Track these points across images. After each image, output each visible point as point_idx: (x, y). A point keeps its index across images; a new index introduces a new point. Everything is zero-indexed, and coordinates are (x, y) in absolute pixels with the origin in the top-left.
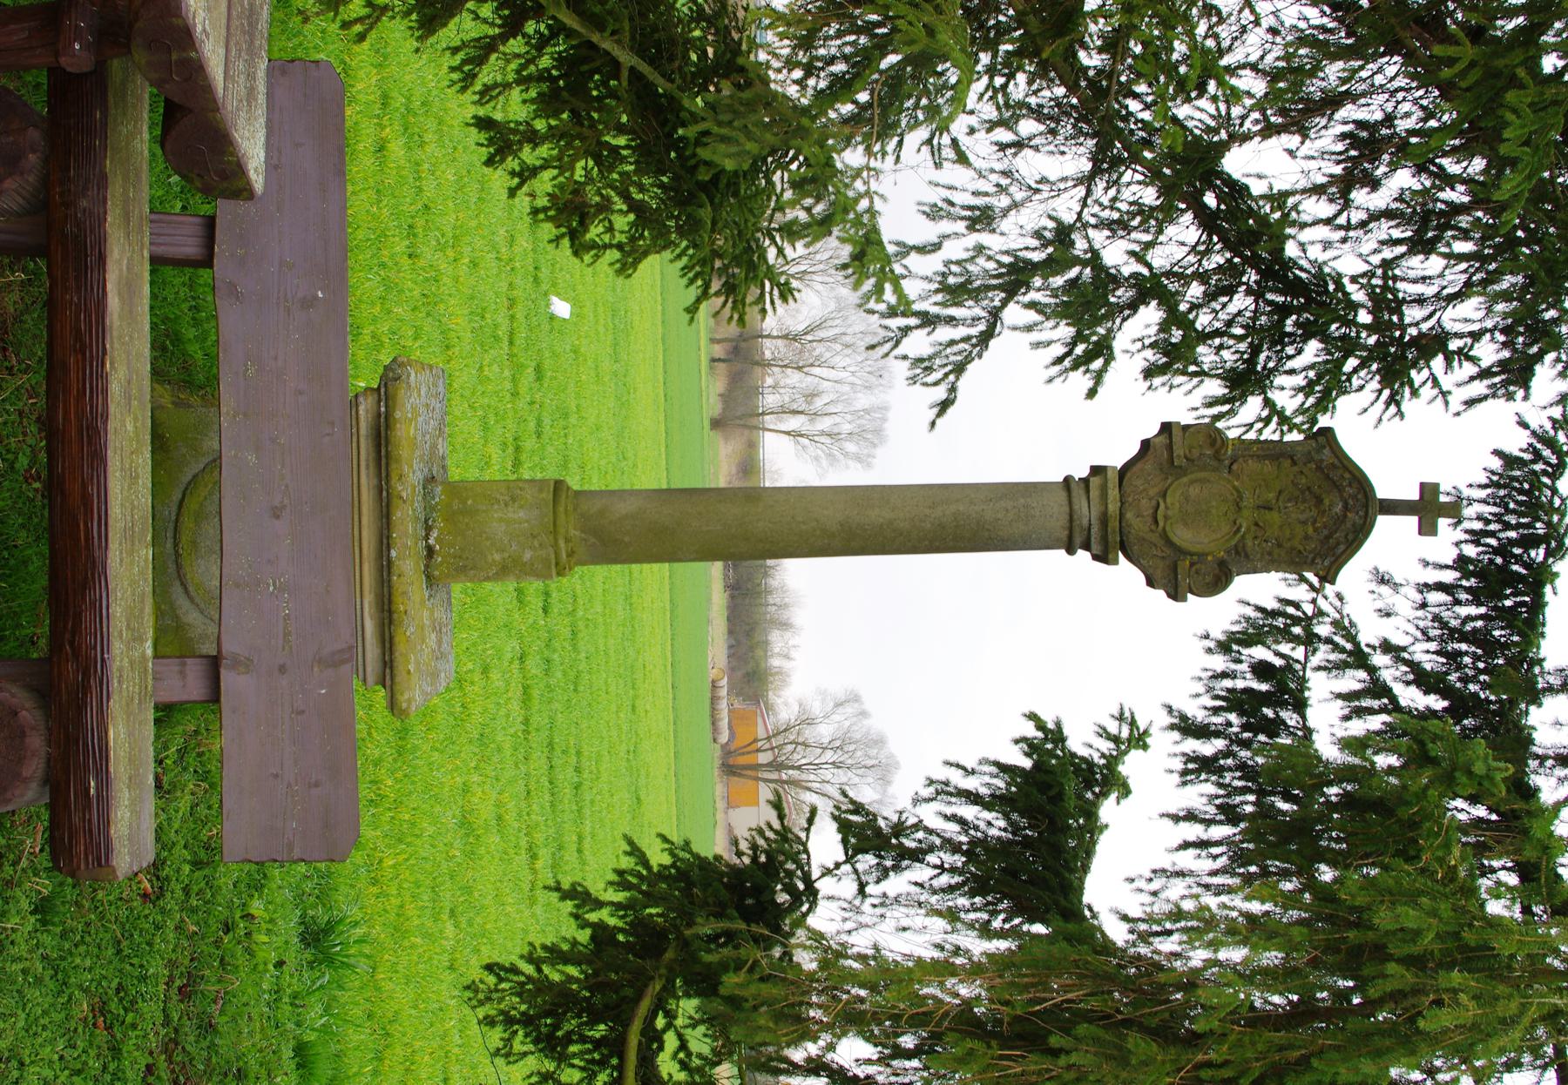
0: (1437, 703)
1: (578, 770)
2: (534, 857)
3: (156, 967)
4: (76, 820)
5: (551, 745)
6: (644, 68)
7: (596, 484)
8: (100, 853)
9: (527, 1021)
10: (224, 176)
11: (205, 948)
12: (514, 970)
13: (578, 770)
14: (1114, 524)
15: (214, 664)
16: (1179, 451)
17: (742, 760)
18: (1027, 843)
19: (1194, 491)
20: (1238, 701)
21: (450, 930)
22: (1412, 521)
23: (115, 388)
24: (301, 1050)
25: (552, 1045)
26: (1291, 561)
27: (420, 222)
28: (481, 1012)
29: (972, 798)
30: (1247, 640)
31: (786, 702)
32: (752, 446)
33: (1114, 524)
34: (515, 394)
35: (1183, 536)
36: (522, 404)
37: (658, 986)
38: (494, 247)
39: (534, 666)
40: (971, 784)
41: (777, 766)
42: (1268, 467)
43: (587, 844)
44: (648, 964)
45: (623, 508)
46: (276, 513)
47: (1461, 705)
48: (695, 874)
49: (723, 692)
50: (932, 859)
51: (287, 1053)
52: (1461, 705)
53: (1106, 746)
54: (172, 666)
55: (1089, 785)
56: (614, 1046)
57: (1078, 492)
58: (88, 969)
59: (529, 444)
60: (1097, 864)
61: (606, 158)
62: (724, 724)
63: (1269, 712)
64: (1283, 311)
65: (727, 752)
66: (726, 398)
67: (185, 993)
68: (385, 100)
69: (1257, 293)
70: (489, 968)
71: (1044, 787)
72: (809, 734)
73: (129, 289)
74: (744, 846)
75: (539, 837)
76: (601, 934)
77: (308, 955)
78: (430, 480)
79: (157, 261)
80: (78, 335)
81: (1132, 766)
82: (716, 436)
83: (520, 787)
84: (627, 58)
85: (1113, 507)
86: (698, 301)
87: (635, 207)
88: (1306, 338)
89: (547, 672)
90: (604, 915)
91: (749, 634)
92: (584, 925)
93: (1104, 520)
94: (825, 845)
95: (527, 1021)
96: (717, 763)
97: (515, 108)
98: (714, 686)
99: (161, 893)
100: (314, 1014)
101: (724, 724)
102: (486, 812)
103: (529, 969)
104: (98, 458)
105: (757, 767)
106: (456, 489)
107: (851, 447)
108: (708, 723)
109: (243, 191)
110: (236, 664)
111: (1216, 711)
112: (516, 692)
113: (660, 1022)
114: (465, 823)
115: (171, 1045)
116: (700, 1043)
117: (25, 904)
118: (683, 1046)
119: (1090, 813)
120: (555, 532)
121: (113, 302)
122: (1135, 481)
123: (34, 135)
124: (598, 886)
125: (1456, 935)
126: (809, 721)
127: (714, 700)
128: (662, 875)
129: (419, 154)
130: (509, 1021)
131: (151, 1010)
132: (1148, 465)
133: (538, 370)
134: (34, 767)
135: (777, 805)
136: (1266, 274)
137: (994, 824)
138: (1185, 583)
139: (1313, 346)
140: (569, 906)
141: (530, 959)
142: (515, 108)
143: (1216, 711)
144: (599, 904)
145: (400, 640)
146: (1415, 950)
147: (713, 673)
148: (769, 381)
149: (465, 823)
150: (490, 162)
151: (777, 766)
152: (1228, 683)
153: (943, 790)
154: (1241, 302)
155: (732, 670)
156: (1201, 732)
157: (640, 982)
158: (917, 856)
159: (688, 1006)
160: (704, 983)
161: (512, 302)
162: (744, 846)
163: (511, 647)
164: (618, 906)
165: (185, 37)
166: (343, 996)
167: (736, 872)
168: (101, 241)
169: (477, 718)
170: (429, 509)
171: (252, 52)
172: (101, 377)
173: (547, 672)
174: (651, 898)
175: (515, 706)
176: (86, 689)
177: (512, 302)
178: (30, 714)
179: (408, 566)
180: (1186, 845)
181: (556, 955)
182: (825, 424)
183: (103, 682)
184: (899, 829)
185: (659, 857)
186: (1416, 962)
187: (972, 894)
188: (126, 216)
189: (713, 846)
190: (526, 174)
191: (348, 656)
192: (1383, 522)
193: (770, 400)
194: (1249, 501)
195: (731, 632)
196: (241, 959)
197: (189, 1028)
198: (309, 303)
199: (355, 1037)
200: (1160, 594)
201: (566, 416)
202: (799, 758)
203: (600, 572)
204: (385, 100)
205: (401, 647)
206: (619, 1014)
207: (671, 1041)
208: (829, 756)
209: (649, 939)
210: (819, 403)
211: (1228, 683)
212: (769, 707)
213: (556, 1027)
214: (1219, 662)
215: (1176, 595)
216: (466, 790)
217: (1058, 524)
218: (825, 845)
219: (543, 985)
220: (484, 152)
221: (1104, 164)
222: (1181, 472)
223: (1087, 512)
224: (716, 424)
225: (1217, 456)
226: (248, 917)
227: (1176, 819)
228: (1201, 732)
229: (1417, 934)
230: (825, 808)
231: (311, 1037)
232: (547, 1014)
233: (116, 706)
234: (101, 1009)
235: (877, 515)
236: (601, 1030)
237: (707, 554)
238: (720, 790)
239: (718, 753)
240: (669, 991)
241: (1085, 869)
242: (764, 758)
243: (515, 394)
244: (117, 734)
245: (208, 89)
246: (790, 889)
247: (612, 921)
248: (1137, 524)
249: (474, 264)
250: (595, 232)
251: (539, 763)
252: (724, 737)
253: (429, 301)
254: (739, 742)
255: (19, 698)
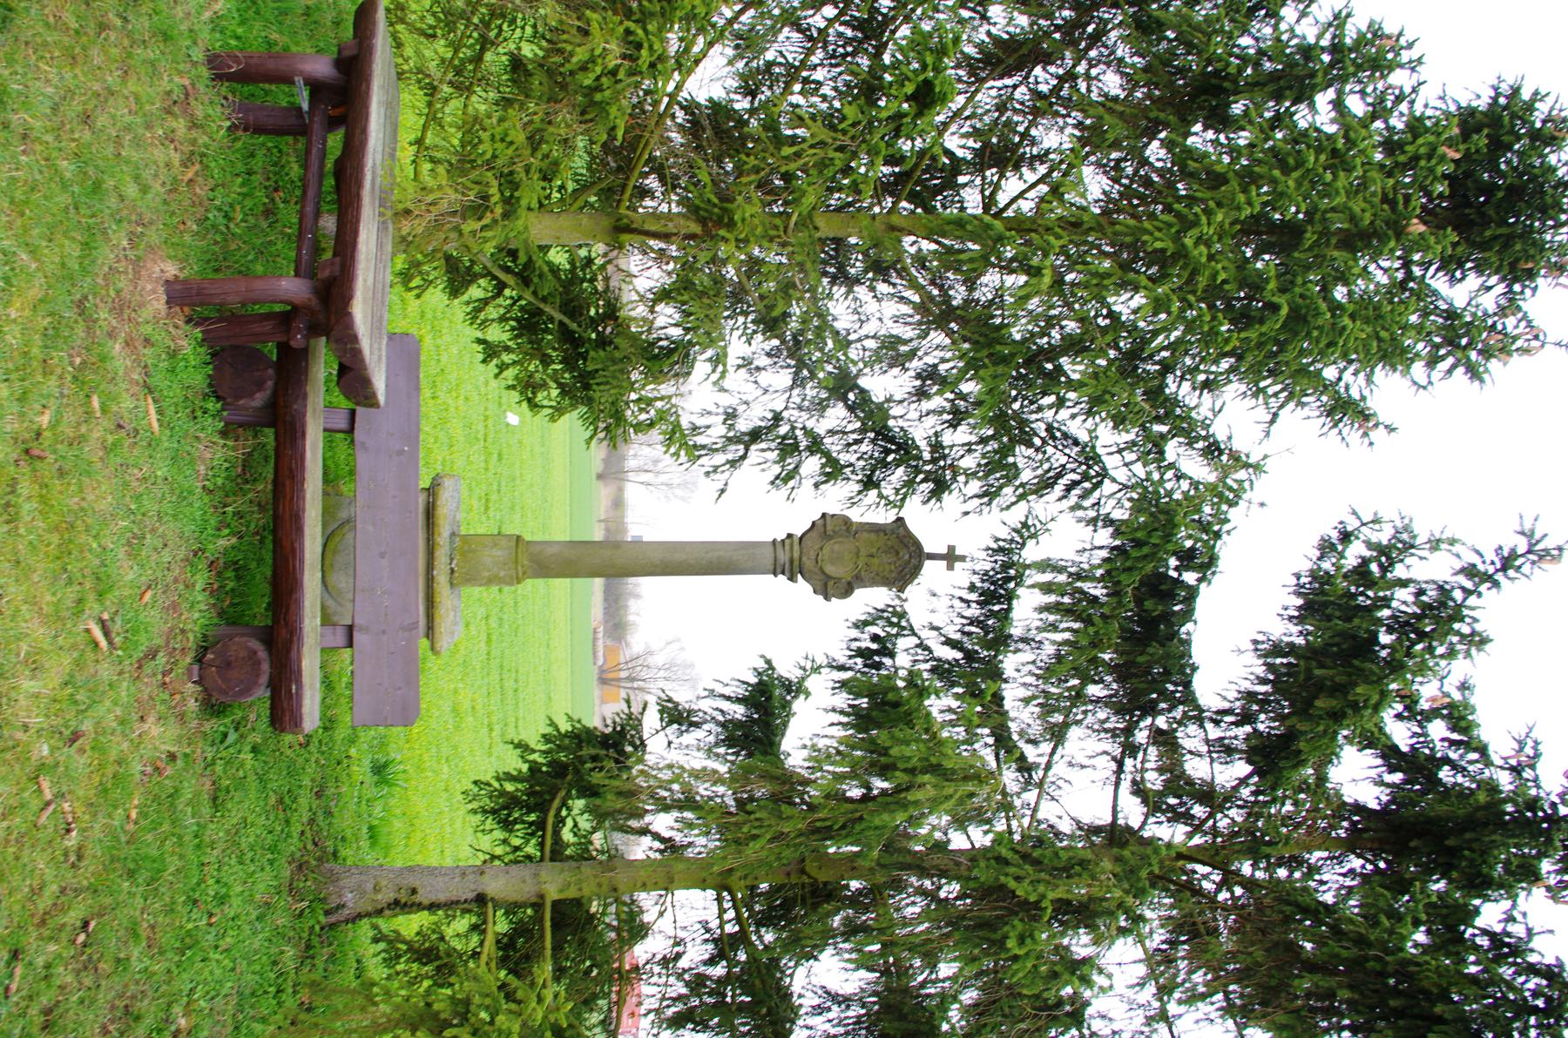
0: (959, 655)
1: (516, 681)
2: (491, 730)
3: (307, 782)
4: (285, 705)
5: (501, 667)
6: (566, 320)
7: (538, 538)
8: (296, 722)
9: (494, 812)
10: (366, 398)
11: (328, 771)
12: (488, 784)
13: (516, 681)
14: (796, 563)
15: (350, 629)
16: (829, 528)
17: (611, 676)
18: (754, 721)
19: (837, 547)
20: (861, 653)
21: (446, 769)
22: (944, 563)
23: (308, 496)
24: (371, 828)
25: (507, 825)
26: (887, 582)
27: (439, 379)
28: (470, 806)
29: (728, 698)
30: (866, 623)
31: (637, 642)
32: (621, 490)
33: (796, 563)
34: (486, 469)
35: (830, 569)
36: (490, 474)
37: (563, 793)
38: (477, 387)
39: (493, 623)
40: (727, 691)
41: (631, 679)
42: (873, 536)
43: (521, 722)
44: (558, 782)
45: (550, 550)
46: (382, 555)
47: (970, 656)
48: (584, 736)
49: (600, 635)
50: (706, 727)
51: (365, 830)
52: (970, 656)
53: (800, 673)
54: (329, 630)
55: (789, 693)
56: (540, 825)
57: (779, 547)
58: (277, 782)
59: (494, 497)
60: (789, 732)
61: (546, 361)
62: (600, 654)
63: (877, 658)
64: (887, 452)
65: (602, 671)
66: (606, 461)
67: (319, 795)
68: (423, 315)
69: (873, 441)
70: (475, 783)
71: (763, 693)
72: (651, 661)
73: (314, 446)
74: (609, 722)
75: (494, 719)
76: (534, 768)
77: (376, 778)
78: (453, 534)
79: (325, 430)
80: (291, 470)
81: (812, 683)
82: (600, 484)
83: (484, 690)
84: (558, 316)
85: (796, 555)
86: (591, 438)
87: (561, 386)
88: (898, 466)
89: (500, 626)
90: (535, 757)
91: (616, 601)
92: (526, 761)
93: (792, 561)
94: (651, 720)
95: (494, 812)
96: (596, 677)
97: (496, 334)
98: (595, 632)
99: (308, 744)
100: (377, 810)
101: (600, 654)
102: (466, 705)
103: (496, 784)
104: (300, 530)
105: (619, 680)
106: (466, 539)
107: (679, 492)
108: (590, 653)
109: (375, 405)
110: (361, 629)
111: (850, 657)
112: (483, 637)
113: (564, 813)
114: (455, 711)
115: (312, 821)
116: (585, 823)
117: (248, 748)
118: (576, 825)
119: (786, 705)
120: (516, 562)
121: (308, 454)
122: (807, 542)
123: (271, 371)
124: (534, 741)
125: (927, 760)
126: (650, 653)
127: (595, 640)
128: (566, 735)
129: (439, 341)
130: (485, 812)
131: (303, 801)
132: (813, 534)
133: (500, 455)
134: (264, 679)
135: (628, 702)
136: (878, 434)
137: (739, 711)
138: (831, 592)
139: (901, 470)
140: (519, 751)
141: (498, 779)
142: (496, 334)
143: (850, 657)
144: (534, 751)
145: (437, 616)
146: (910, 766)
147: (594, 624)
148: (632, 452)
149: (455, 711)
150: (484, 361)
151: (631, 679)
152: (857, 644)
153: (712, 693)
154: (865, 447)
155: (606, 622)
156: (842, 668)
157: (553, 793)
158: (697, 725)
159: (579, 804)
160: (590, 791)
161: (486, 418)
162: (609, 722)
163: (481, 612)
164: (544, 752)
165: (354, 338)
166: (392, 802)
167: (605, 736)
168: (303, 426)
169: (463, 652)
170: (452, 549)
171: (381, 338)
172: (302, 490)
173: (500, 626)
174: (560, 748)
175: (483, 644)
176: (291, 641)
177: (486, 418)
178: (262, 654)
179: (441, 578)
180: (832, 724)
181: (510, 777)
182: (663, 478)
183: (300, 639)
184: (690, 712)
185: (565, 727)
186: (912, 771)
187: (730, 747)
188: (314, 411)
189: (594, 722)
190: (502, 367)
191: (415, 626)
192: (928, 564)
193: (631, 463)
194: (863, 552)
195: (606, 600)
196: (344, 777)
197: (320, 813)
198: (401, 453)
199: (397, 824)
200: (821, 598)
201: (514, 480)
202: (643, 675)
203: (540, 582)
204: (423, 315)
205: (437, 620)
206: (542, 807)
207: (569, 823)
208: (662, 673)
209: (559, 769)
210: (660, 466)
211: (857, 644)
212: (627, 645)
213: (509, 815)
214: (855, 633)
215: (827, 598)
216: (456, 691)
217: (769, 562)
218: (651, 720)
219: (503, 793)
220: (481, 357)
221: (798, 382)
222: (830, 538)
223: (783, 557)
224: (600, 477)
225: (848, 530)
226: (348, 757)
227: (826, 710)
228: (842, 668)
229: (910, 758)
230: (652, 700)
231: (376, 822)
232: (504, 808)
233: (306, 650)
234: (281, 801)
235: (679, 557)
236: (532, 817)
237: (594, 574)
238: (597, 693)
239: (595, 671)
240: (568, 796)
241: (783, 735)
242: (623, 674)
243: (486, 469)
244: (305, 664)
245: (363, 360)
246: (632, 744)
247: (541, 760)
248: (808, 563)
249: (467, 399)
250: (540, 396)
251: (495, 676)
252: (600, 662)
253: (443, 421)
254: (611, 664)
255: (256, 645)
